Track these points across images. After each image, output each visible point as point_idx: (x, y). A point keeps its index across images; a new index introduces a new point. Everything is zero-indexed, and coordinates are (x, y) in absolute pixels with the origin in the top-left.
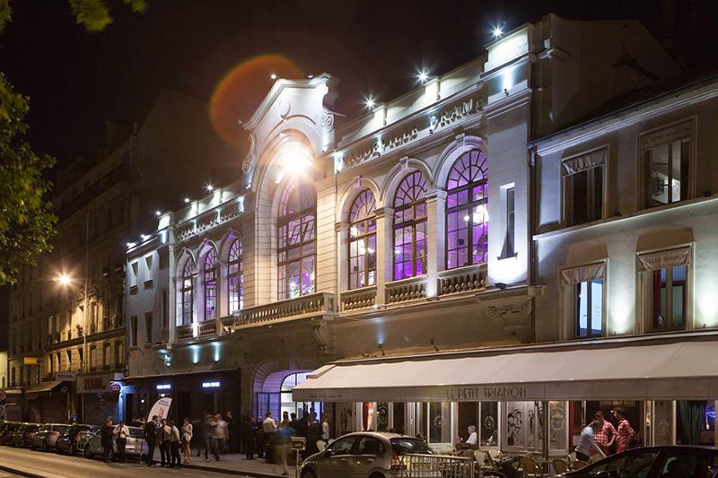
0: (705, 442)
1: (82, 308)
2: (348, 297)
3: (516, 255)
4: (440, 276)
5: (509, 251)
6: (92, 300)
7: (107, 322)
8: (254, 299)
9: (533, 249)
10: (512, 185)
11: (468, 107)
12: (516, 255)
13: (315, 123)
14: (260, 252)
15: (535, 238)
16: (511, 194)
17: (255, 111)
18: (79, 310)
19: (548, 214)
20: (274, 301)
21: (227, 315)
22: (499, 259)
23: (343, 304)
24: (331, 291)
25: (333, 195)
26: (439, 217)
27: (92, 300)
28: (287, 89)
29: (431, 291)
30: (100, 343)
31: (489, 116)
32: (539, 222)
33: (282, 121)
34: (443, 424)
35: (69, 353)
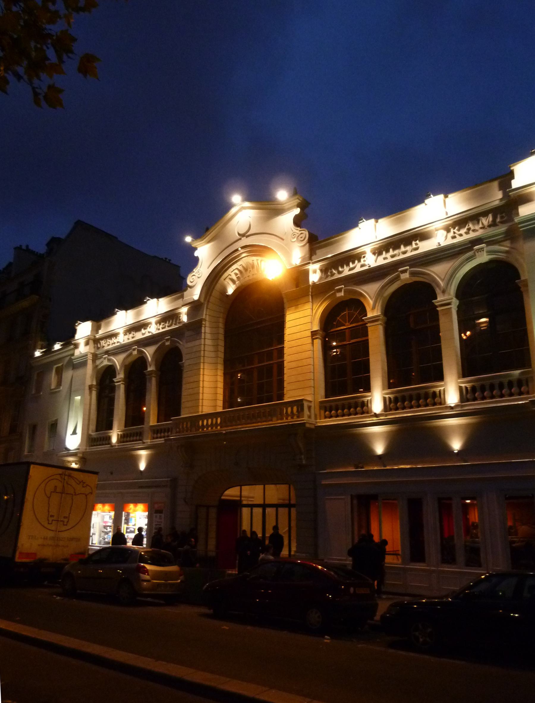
0: (392, 556)
2: (328, 405)
4: (387, 394)
8: (198, 406)
11: (485, 221)
13: (283, 239)
14: (207, 360)
20: (220, 409)
23: (322, 412)
24: (309, 398)
25: (311, 303)
28: (244, 212)
29: (114, 440)
31: (522, 227)
33: (240, 239)
34: (56, 378)
35: (310, 417)
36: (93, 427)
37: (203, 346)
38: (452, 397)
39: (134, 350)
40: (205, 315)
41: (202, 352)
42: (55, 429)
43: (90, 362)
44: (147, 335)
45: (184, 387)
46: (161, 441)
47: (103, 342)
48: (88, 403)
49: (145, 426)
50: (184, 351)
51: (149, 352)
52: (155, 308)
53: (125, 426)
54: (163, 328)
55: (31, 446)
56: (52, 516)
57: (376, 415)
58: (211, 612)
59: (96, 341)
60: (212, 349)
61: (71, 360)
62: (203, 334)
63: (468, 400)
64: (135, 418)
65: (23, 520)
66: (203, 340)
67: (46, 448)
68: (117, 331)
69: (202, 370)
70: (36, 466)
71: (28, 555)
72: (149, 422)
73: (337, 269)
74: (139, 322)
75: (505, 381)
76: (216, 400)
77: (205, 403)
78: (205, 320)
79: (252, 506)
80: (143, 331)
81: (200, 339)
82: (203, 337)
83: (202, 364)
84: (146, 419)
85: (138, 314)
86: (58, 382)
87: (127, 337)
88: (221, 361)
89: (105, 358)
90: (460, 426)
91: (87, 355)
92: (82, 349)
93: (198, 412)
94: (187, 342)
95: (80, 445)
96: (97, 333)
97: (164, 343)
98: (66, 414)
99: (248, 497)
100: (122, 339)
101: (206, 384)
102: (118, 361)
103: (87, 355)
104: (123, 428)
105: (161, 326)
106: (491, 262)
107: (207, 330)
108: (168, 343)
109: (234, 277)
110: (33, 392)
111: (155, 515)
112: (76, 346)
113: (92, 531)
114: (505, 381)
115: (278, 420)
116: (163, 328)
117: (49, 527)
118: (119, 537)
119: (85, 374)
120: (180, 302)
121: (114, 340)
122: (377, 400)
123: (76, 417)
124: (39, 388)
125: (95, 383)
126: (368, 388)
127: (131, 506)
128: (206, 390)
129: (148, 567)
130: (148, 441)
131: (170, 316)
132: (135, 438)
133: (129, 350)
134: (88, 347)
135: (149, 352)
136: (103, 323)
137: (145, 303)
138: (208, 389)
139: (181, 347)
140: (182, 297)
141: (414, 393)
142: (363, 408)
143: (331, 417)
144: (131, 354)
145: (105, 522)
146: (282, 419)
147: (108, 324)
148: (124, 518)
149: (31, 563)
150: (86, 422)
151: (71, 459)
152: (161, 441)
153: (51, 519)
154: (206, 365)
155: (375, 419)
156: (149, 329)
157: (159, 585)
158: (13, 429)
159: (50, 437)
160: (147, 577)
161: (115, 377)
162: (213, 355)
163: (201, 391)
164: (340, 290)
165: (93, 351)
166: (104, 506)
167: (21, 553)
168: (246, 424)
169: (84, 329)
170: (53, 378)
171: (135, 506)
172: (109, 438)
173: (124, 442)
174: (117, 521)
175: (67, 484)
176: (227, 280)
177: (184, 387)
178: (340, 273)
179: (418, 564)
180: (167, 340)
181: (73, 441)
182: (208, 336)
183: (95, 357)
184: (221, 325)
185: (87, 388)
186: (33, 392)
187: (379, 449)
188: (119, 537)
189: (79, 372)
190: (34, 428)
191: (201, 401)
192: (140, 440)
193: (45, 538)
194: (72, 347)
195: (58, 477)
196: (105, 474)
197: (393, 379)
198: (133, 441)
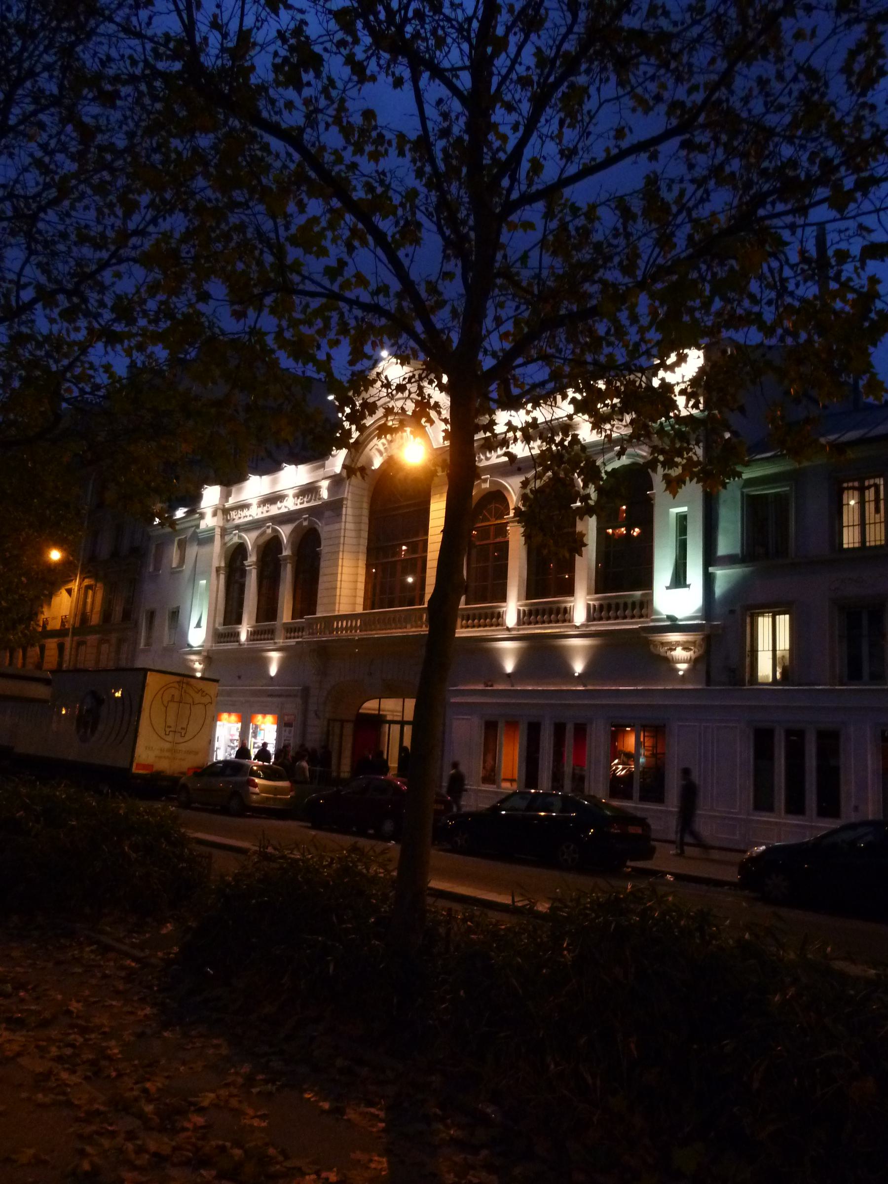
1: (69, 592)
3: (689, 586)
5: (679, 580)
6: (87, 582)
7: (106, 616)
8: (334, 604)
9: (709, 581)
10: (684, 509)
12: (689, 586)
13: (216, 681)
15: (711, 569)
16: (682, 520)
17: (277, 603)
18: (64, 593)
19: (725, 546)
20: (359, 609)
21: (406, 700)
22: (668, 588)
26: (359, 584)
27: (87, 582)
30: (92, 639)
32: (716, 552)
34: (179, 552)
36: (220, 619)
37: (342, 531)
38: (580, 616)
39: (268, 527)
40: (348, 492)
41: (342, 539)
42: (176, 617)
43: (217, 538)
44: (284, 510)
45: (321, 579)
46: (292, 642)
47: (233, 513)
48: (215, 589)
49: (278, 623)
50: (323, 536)
51: (285, 532)
52: (293, 476)
53: (257, 622)
54: (301, 504)
55: (149, 637)
56: (170, 727)
57: (508, 629)
58: (309, 825)
59: (226, 511)
60: (353, 534)
61: (195, 533)
62: (344, 517)
63: (594, 620)
64: (267, 611)
65: (140, 730)
66: (343, 524)
67: (166, 642)
68: (249, 501)
69: (340, 561)
70: (154, 673)
71: (145, 766)
72: (282, 619)
73: (485, 454)
74: (276, 491)
75: (630, 601)
76: (355, 596)
77: (344, 600)
78: (347, 499)
79: (392, 722)
80: (279, 504)
81: (341, 522)
82: (343, 520)
83: (341, 553)
84: (279, 615)
85: (274, 482)
86: (180, 558)
87: (260, 510)
88: (363, 549)
89: (235, 534)
90: (584, 647)
91: (214, 529)
92: (209, 522)
93: (334, 610)
94: (326, 525)
95: (204, 642)
96: (227, 501)
97: (301, 523)
98: (189, 603)
99: (392, 711)
100: (256, 512)
101: (345, 577)
102: (249, 539)
103: (214, 529)
104: (253, 623)
105: (299, 501)
106: (633, 464)
107: (348, 511)
108: (305, 523)
109: (382, 448)
110: (151, 569)
111: (284, 729)
112: (202, 516)
113: (217, 745)
114: (630, 601)
115: (412, 627)
116: (301, 504)
117: (165, 737)
118: (243, 752)
119: (212, 553)
120: (321, 472)
121: (246, 512)
122: (511, 610)
123: (201, 606)
124: (157, 568)
125: (223, 565)
126: (503, 598)
127: (259, 717)
128: (344, 585)
129: (257, 780)
130: (280, 641)
131: (309, 490)
132: (266, 636)
133: (261, 527)
134: (215, 519)
135: (285, 532)
136: (234, 489)
137: (283, 469)
138: (347, 584)
139: (320, 530)
140: (323, 466)
141: (547, 607)
142: (497, 618)
143: (467, 627)
144: (264, 533)
145: (232, 735)
146: (421, 627)
147: (239, 491)
148: (251, 731)
149: (146, 774)
150: (213, 613)
151: (194, 657)
152: (292, 642)
153: (168, 730)
154: (345, 554)
155: (507, 633)
156: (285, 503)
157: (267, 798)
158: (127, 615)
159: (170, 628)
160: (257, 790)
161: (246, 560)
162: (354, 541)
163: (338, 586)
164: (485, 481)
165: (221, 524)
166: (230, 716)
167: (138, 765)
168: (380, 630)
169: (211, 495)
170: (174, 553)
171: (264, 718)
172: (238, 634)
173: (254, 640)
174: (244, 734)
175: (185, 692)
176: (374, 450)
177: (322, 579)
178: (487, 459)
179: (763, 814)
180: (305, 519)
181: (197, 636)
182: (350, 519)
183: (224, 531)
184: (366, 506)
185: (214, 570)
186: (151, 569)
187: (509, 666)
188: (243, 752)
189: (205, 550)
190: (151, 615)
191: (338, 597)
192: (272, 639)
193: (162, 750)
194: (197, 515)
195: (176, 685)
196: (233, 678)
197: (532, 589)
198: (264, 640)
